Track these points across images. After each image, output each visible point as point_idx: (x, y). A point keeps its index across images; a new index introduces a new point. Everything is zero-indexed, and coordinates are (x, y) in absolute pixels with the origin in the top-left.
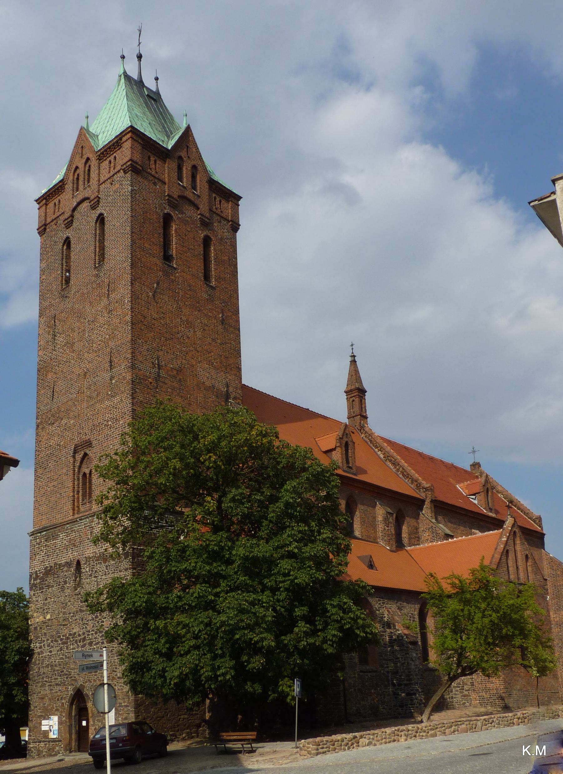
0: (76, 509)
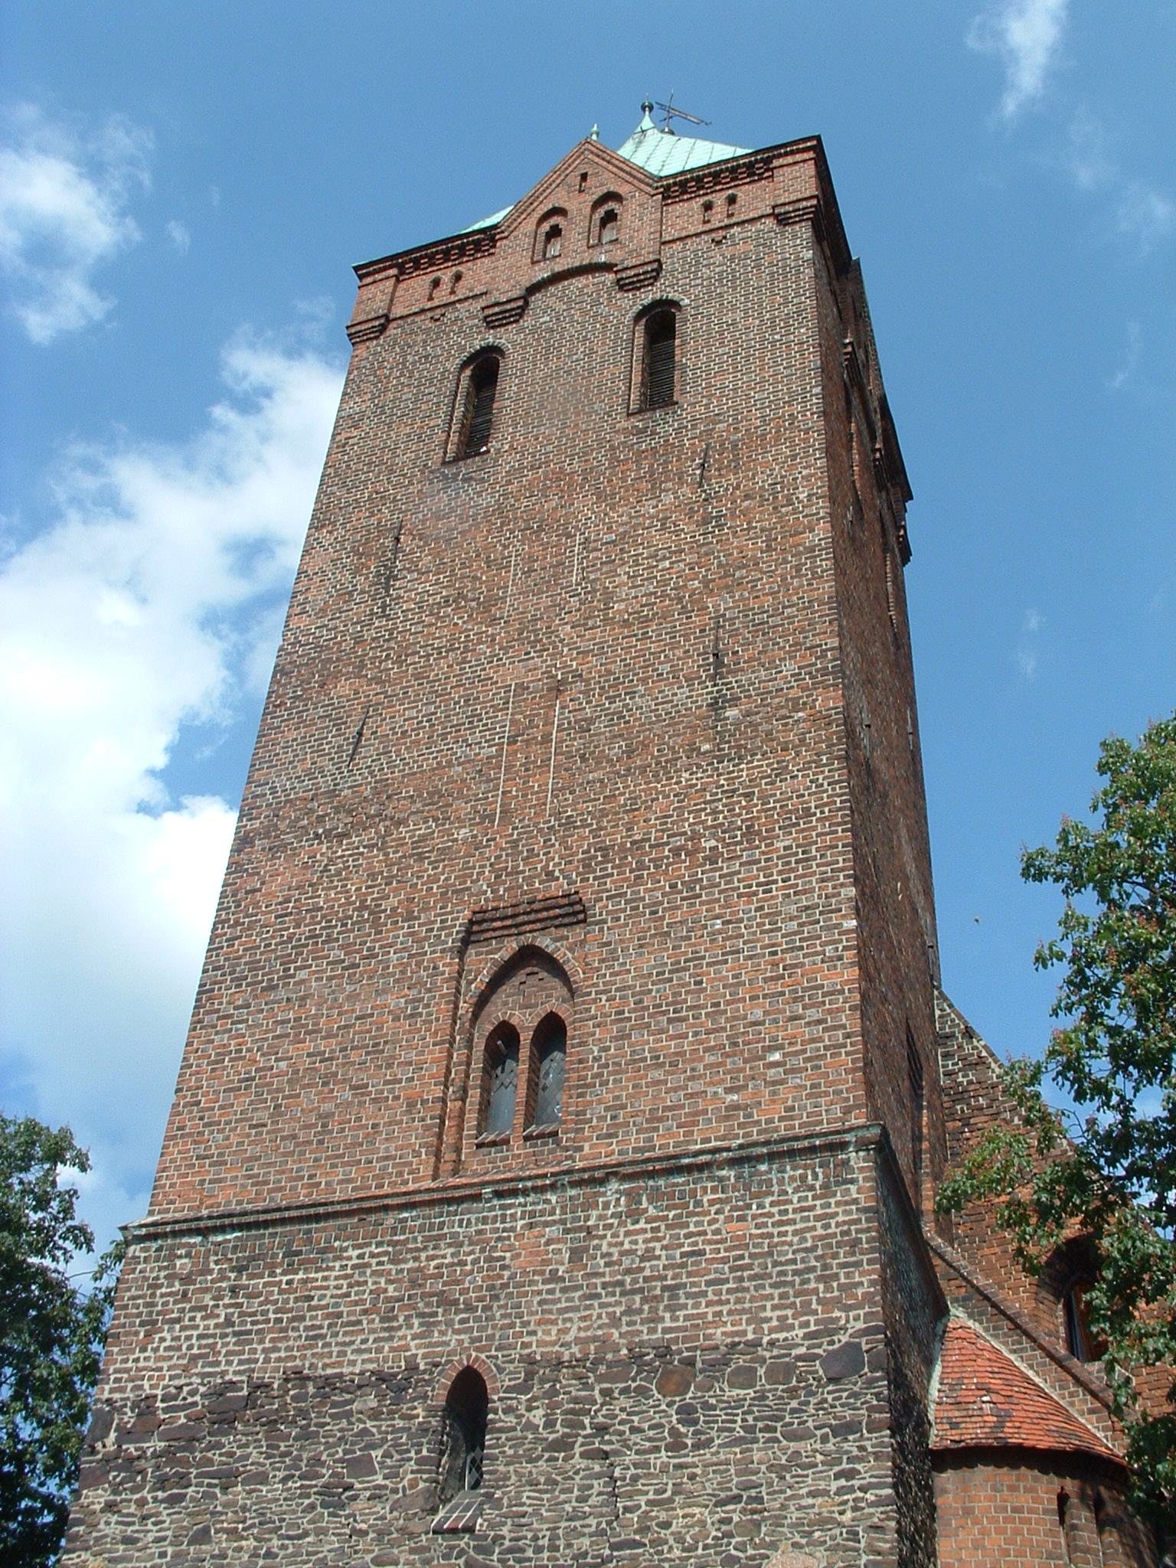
0: (449, 1156)
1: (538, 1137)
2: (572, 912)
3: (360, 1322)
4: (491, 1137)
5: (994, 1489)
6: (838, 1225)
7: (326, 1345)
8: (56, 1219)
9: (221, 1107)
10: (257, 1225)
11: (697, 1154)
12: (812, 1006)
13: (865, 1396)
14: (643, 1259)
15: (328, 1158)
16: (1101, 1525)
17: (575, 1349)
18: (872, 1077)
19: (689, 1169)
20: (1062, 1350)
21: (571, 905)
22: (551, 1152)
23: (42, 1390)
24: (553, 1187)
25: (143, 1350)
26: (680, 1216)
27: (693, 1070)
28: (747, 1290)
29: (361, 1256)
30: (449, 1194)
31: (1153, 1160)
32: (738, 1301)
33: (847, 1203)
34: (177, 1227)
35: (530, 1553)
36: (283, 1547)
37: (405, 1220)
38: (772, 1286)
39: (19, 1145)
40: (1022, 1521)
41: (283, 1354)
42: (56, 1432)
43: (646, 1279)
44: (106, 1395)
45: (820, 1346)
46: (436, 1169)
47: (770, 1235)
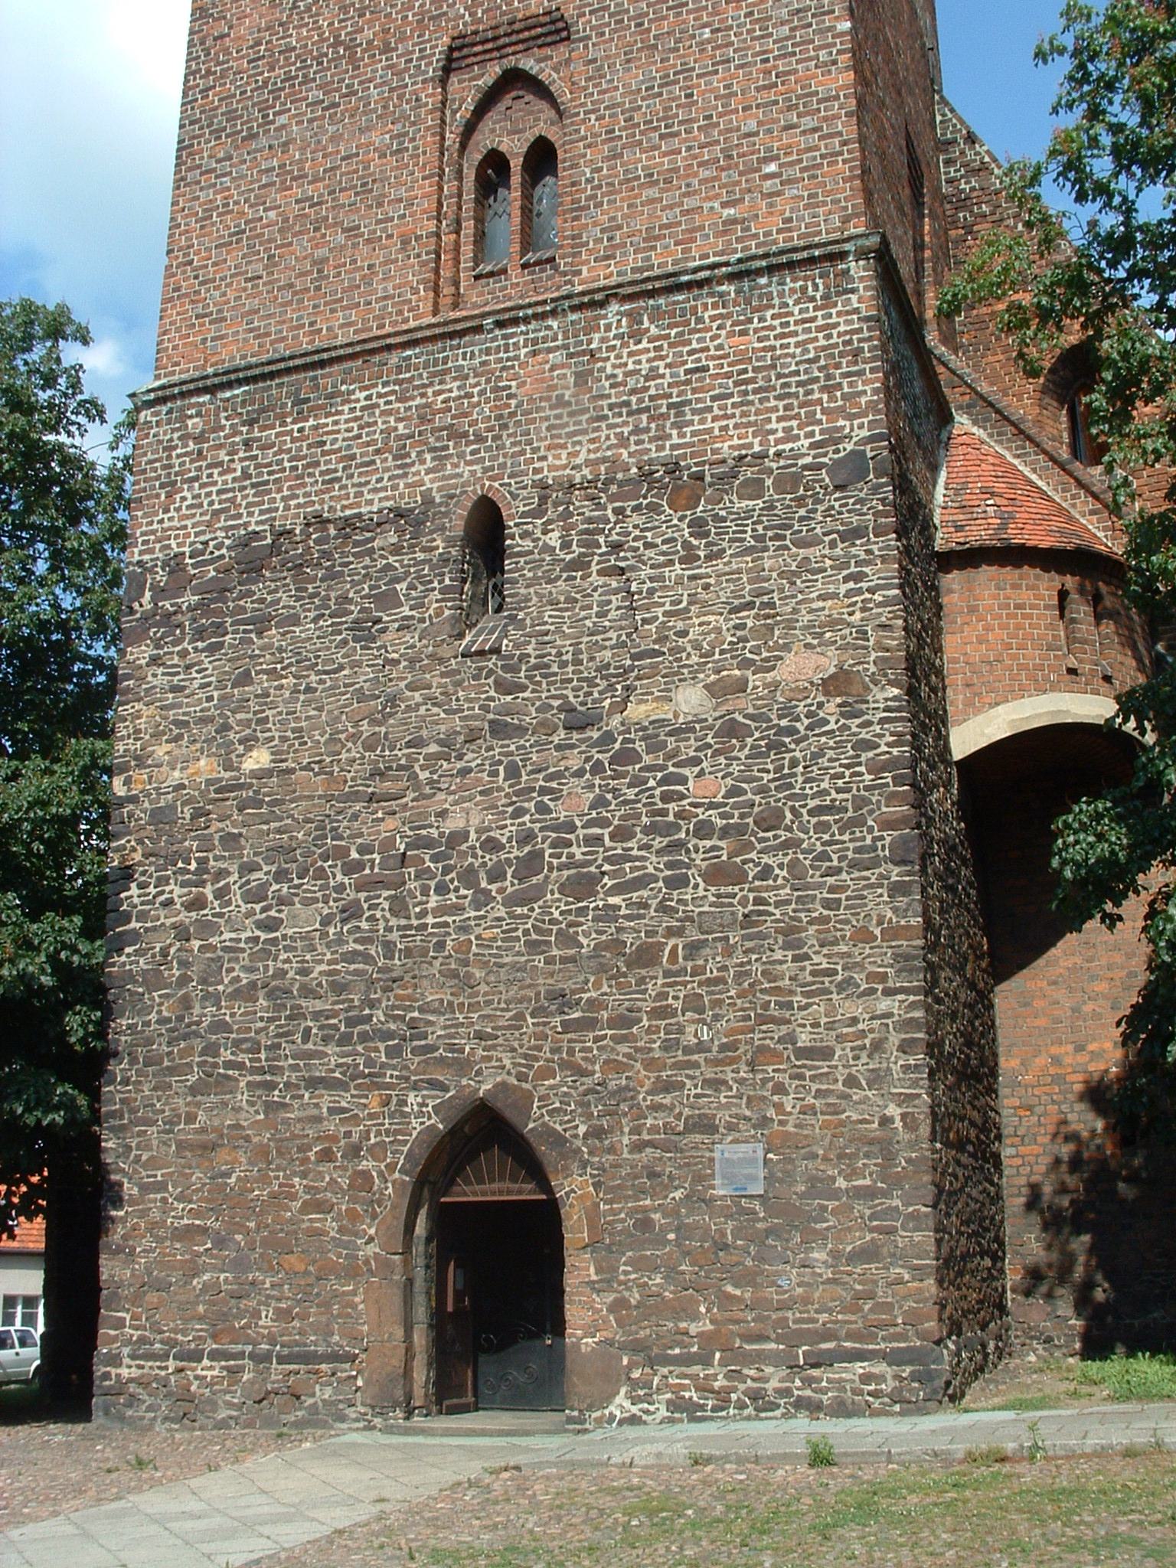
0: (447, 290)
1: (536, 264)
2: (555, 30)
3: (373, 462)
4: (489, 268)
5: (998, 588)
6: (839, 335)
7: (343, 487)
8: (65, 395)
9: (215, 264)
10: (263, 377)
11: (696, 270)
12: (807, 113)
13: (873, 500)
14: (647, 378)
15: (326, 304)
16: (1098, 618)
17: (586, 471)
18: (871, 185)
19: (689, 286)
20: (1064, 454)
21: (553, 22)
22: (549, 278)
23: (76, 560)
24: (553, 313)
25: (166, 511)
26: (682, 334)
27: (688, 185)
28: (752, 403)
29: (368, 398)
30: (451, 328)
31: (1155, 261)
32: (744, 414)
33: (848, 313)
34: (184, 388)
35: (555, 669)
36: (321, 682)
37: (409, 358)
38: (776, 398)
39: (18, 327)
40: (1024, 616)
41: (301, 500)
42: (95, 599)
43: (652, 398)
44: (137, 558)
45: (825, 455)
46: (436, 304)
47: (773, 348)
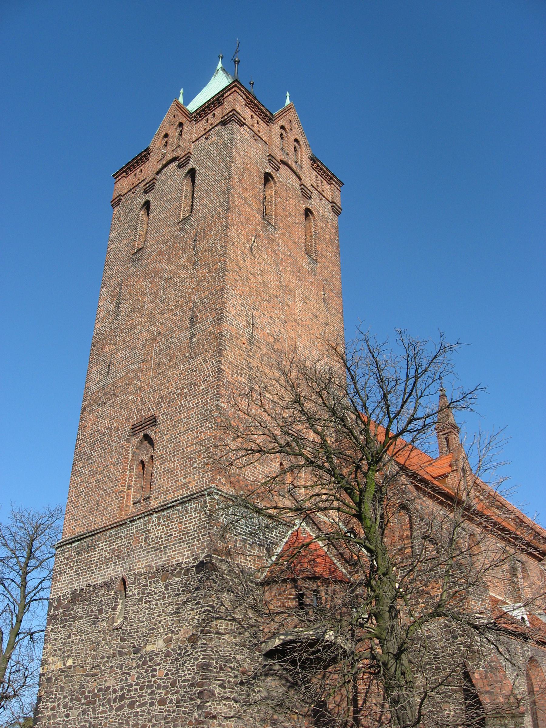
2: (153, 421)
35: (133, 634)
